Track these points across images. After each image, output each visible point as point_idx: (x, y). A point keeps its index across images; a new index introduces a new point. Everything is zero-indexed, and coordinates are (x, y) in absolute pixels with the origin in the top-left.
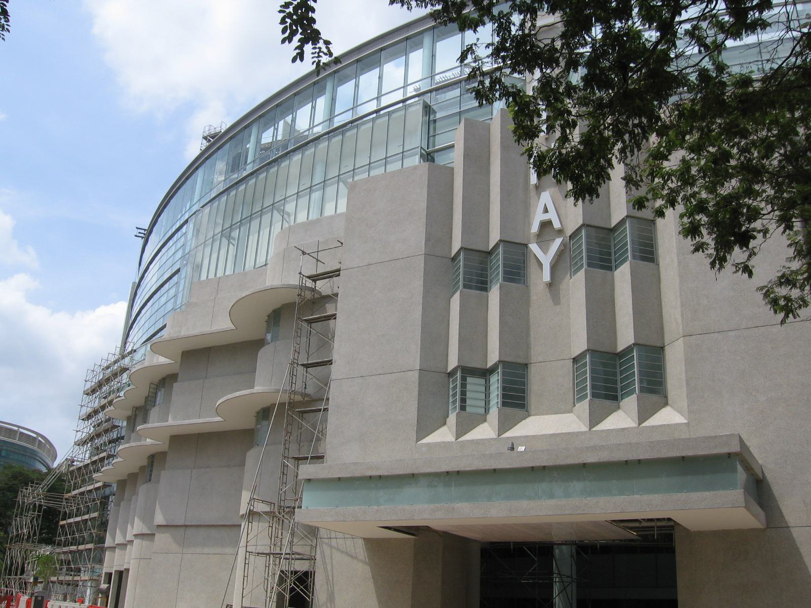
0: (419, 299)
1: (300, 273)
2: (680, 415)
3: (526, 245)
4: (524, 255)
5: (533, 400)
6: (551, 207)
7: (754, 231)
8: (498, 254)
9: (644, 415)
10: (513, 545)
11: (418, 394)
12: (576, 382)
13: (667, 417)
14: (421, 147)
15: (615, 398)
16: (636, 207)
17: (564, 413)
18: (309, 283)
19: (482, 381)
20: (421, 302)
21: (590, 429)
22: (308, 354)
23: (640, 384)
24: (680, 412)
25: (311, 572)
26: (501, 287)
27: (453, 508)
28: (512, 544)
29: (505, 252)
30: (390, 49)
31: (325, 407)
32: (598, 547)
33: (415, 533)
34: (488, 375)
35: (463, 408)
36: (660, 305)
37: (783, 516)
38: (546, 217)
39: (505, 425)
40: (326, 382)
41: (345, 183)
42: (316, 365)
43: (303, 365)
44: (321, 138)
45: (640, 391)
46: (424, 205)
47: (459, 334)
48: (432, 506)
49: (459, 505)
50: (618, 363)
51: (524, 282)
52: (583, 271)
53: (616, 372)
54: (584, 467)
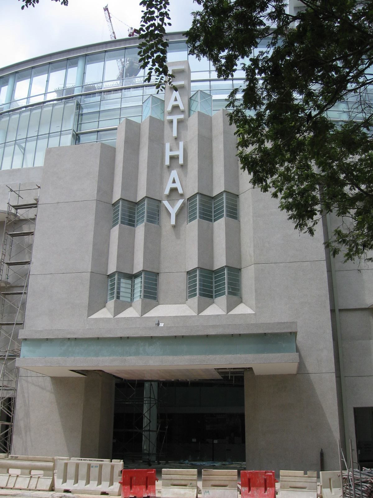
0: (91, 227)
1: (8, 203)
2: (250, 309)
3: (160, 201)
4: (158, 207)
5: (161, 295)
6: (177, 180)
7: (316, 211)
8: (144, 205)
9: (230, 307)
10: (137, 381)
11: (90, 287)
12: (188, 286)
13: (242, 309)
14: (73, 130)
15: (211, 297)
16: (263, 190)
17: (181, 304)
18: (13, 211)
19: (130, 282)
20: (93, 230)
21: (198, 314)
22: (10, 256)
23: (228, 289)
24: (250, 307)
25: (13, 398)
26: (145, 225)
27: (125, 360)
28: (137, 381)
29: (148, 204)
30: (55, 64)
31: (25, 292)
32: (190, 383)
33: (86, 374)
34: (133, 278)
35: (118, 297)
36: (240, 245)
37: (306, 367)
38: (174, 186)
39: (145, 309)
40: (26, 275)
41: (20, 146)
42: (17, 264)
43: (7, 263)
44: (3, 115)
45: (228, 293)
46: (97, 169)
47: (118, 252)
48: (111, 358)
49: (129, 358)
50: (214, 276)
51: (159, 224)
52: (197, 220)
53: (212, 282)
54: (207, 337)
